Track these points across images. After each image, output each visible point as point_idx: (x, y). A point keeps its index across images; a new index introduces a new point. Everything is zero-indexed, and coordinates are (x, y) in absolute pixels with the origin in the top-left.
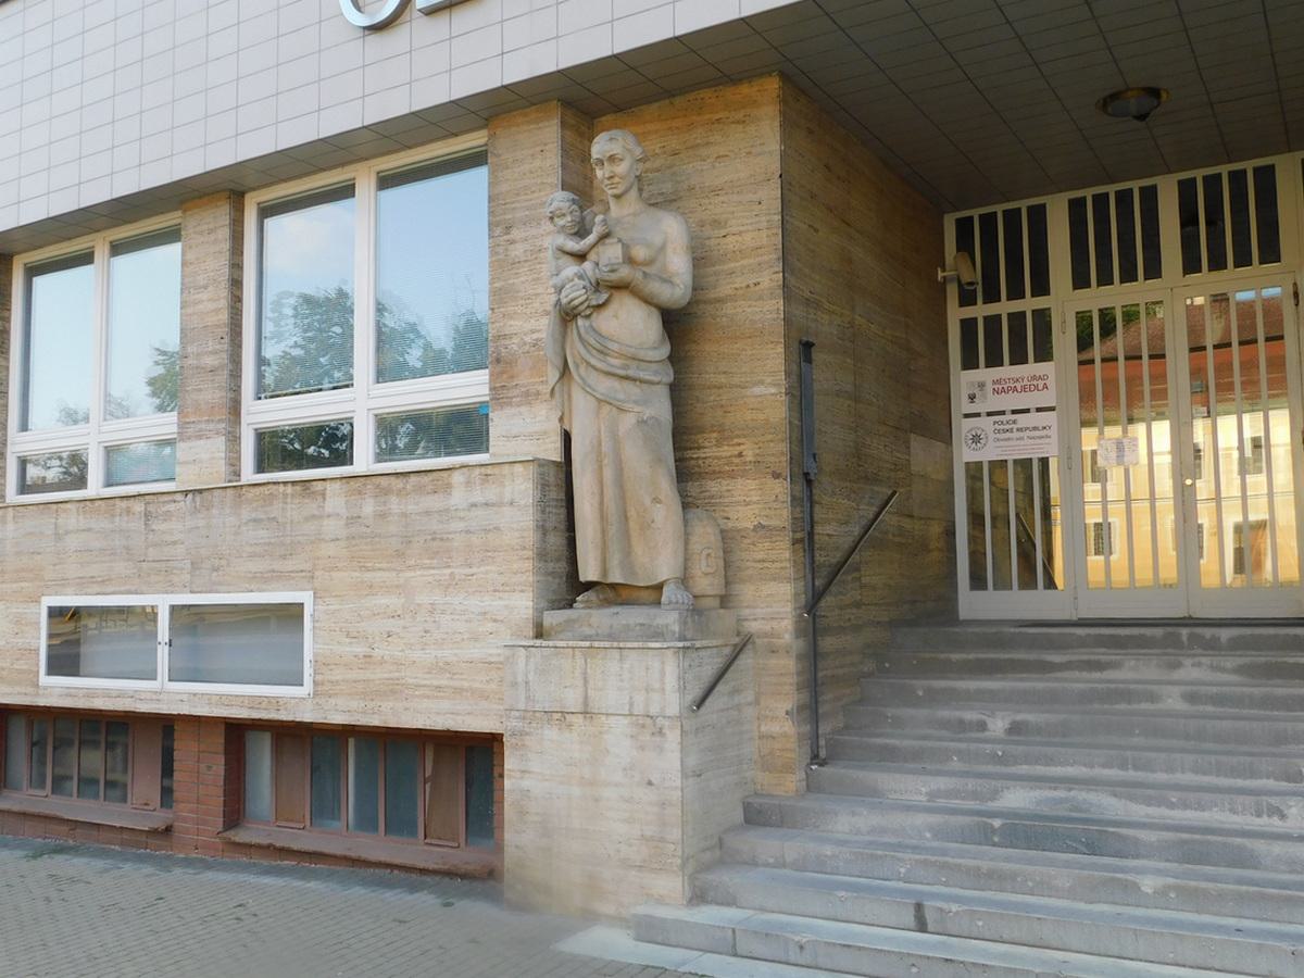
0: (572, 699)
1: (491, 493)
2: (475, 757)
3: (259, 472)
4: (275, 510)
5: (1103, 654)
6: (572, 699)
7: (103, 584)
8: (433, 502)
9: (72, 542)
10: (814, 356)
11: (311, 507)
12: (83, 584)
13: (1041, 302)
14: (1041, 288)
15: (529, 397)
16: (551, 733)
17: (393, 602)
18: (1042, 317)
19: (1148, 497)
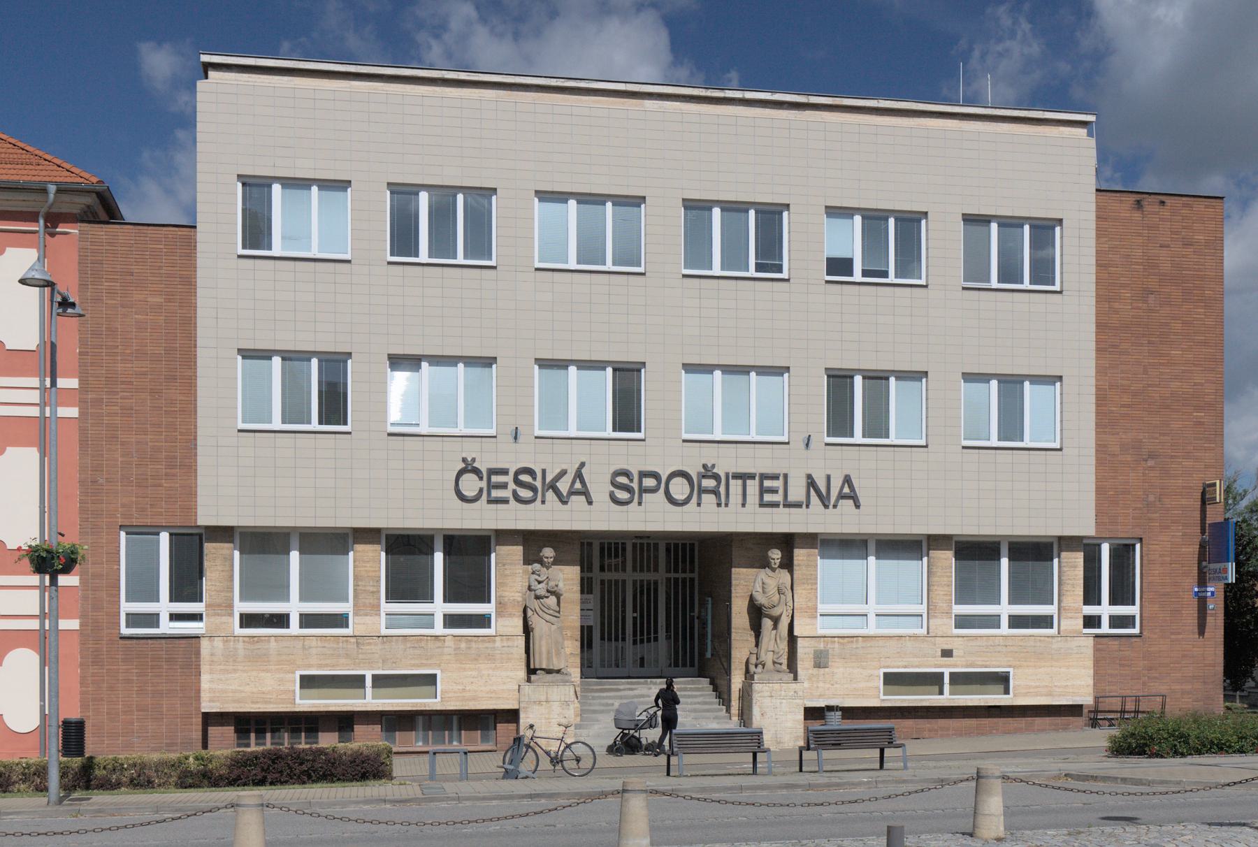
0: (543, 698)
1: (510, 643)
2: (512, 716)
3: (127, 615)
4: (423, 644)
5: (741, 788)
6: (543, 698)
7: (333, 667)
8: (490, 645)
9: (314, 651)
10: (71, 300)
11: (439, 644)
12: (320, 666)
13: (669, 575)
14: (668, 580)
15: (511, 615)
16: (536, 707)
17: (474, 673)
18: (668, 571)
19: (799, 641)
